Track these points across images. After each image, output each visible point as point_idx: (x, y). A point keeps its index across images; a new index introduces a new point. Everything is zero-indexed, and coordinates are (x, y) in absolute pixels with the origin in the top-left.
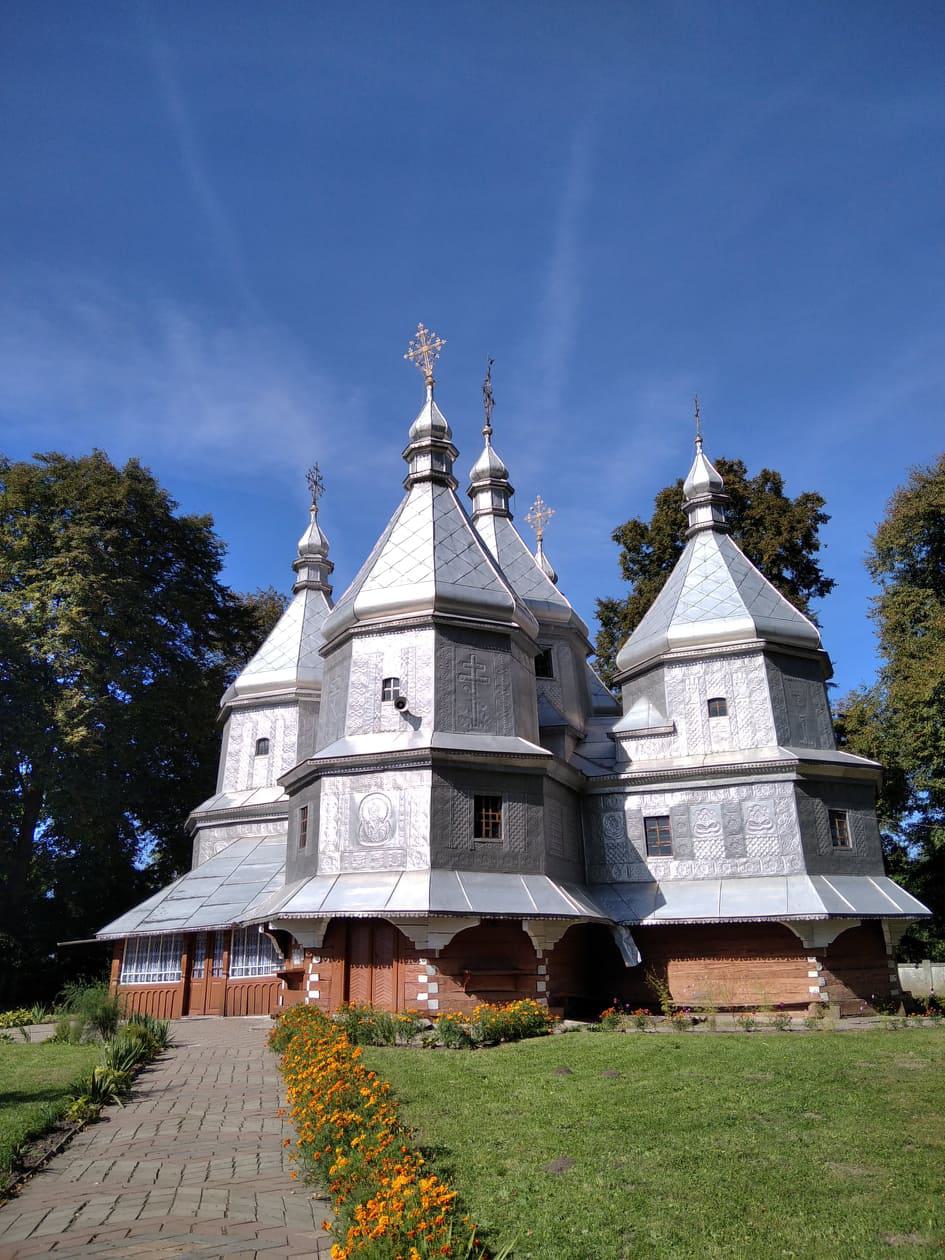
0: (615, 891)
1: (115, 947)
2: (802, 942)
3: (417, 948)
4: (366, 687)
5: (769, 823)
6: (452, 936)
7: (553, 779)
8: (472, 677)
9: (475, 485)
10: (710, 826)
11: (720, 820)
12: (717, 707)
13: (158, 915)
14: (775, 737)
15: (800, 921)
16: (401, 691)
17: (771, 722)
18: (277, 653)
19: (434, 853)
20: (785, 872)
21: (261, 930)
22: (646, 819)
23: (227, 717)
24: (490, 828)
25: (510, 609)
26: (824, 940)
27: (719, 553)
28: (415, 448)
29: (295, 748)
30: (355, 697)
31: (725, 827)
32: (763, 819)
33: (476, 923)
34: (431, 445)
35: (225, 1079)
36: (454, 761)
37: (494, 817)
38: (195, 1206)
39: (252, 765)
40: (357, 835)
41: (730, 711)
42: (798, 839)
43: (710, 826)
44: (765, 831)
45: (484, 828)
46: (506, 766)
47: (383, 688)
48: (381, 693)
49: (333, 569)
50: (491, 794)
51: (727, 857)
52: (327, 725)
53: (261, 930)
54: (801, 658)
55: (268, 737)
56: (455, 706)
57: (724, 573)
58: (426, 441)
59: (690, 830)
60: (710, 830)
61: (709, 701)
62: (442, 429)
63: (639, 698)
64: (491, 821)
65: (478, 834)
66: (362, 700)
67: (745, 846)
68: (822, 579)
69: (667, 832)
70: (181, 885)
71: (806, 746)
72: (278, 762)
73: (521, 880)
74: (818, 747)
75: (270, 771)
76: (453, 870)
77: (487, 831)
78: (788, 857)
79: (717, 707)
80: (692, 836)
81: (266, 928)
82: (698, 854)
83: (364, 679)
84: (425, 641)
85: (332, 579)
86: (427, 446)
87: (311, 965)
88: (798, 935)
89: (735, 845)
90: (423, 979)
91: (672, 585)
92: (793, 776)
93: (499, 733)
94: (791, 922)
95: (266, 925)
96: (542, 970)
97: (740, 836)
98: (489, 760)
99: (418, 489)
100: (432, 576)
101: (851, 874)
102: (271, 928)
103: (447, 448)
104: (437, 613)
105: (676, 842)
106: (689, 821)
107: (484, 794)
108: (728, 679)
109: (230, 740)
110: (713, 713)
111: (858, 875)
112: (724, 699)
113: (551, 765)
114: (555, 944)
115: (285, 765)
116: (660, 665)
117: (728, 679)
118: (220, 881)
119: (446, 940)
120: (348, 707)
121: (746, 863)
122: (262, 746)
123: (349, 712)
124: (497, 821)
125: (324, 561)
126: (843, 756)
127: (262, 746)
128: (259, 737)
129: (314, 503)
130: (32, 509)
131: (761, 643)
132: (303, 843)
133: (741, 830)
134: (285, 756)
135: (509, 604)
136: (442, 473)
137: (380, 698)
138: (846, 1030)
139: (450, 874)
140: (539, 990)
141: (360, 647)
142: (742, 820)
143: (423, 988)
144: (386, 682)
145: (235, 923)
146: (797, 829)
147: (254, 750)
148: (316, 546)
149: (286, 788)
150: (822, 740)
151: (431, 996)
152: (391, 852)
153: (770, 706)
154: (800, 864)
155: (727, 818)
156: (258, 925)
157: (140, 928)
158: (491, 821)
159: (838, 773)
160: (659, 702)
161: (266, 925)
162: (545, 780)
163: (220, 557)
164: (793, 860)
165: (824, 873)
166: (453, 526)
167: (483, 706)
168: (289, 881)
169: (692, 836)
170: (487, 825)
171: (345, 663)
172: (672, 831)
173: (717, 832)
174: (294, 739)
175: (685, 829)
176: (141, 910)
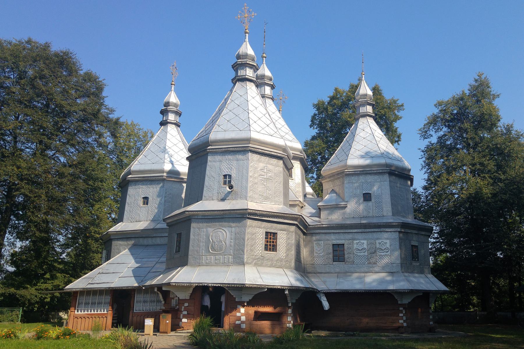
0: (318, 277)
1: (75, 294)
3: (237, 300)
6: (253, 295)
8: (265, 177)
13: (96, 280)
15: (182, 286)
22: (333, 245)
26: (406, 301)
28: (239, 64)
33: (422, 294)
37: (267, 242)
44: (385, 253)
45: (269, 247)
50: (273, 231)
60: (362, 251)
61: (363, 194)
65: (266, 249)
68: (79, 73)
77: (270, 248)
82: (356, 262)
87: (183, 307)
88: (396, 298)
90: (401, 315)
92: (399, 230)
94: (393, 292)
96: (290, 311)
105: (346, 256)
114: (296, 300)
116: (245, 151)
118: (148, 269)
119: (250, 297)
122: (146, 200)
124: (275, 244)
127: (146, 200)
132: (178, 251)
138: (431, 335)
140: (169, 316)
142: (376, 248)
143: (402, 318)
144: (225, 176)
157: (87, 287)
158: (272, 244)
163: (497, 107)
173: (364, 252)
176: (315, 285)
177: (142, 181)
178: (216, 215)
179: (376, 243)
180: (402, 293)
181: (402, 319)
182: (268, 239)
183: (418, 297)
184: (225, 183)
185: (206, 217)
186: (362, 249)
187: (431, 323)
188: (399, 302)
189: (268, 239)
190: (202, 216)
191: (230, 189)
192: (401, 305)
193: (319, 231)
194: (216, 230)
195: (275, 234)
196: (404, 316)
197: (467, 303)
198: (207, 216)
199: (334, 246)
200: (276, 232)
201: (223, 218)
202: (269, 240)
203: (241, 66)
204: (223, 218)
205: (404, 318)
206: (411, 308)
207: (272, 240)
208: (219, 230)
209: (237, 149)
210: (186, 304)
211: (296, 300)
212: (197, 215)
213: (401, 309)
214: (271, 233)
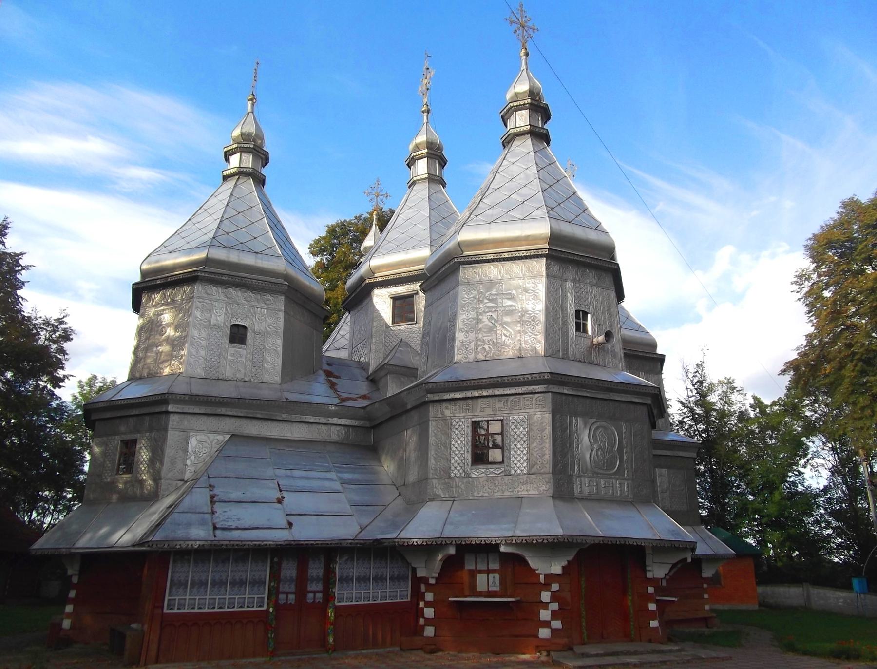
12: (238, 334)
22: (654, 455)
112: (245, 328)
151: (546, 624)
199: (501, 460)
210: (555, 587)
211: (563, 567)
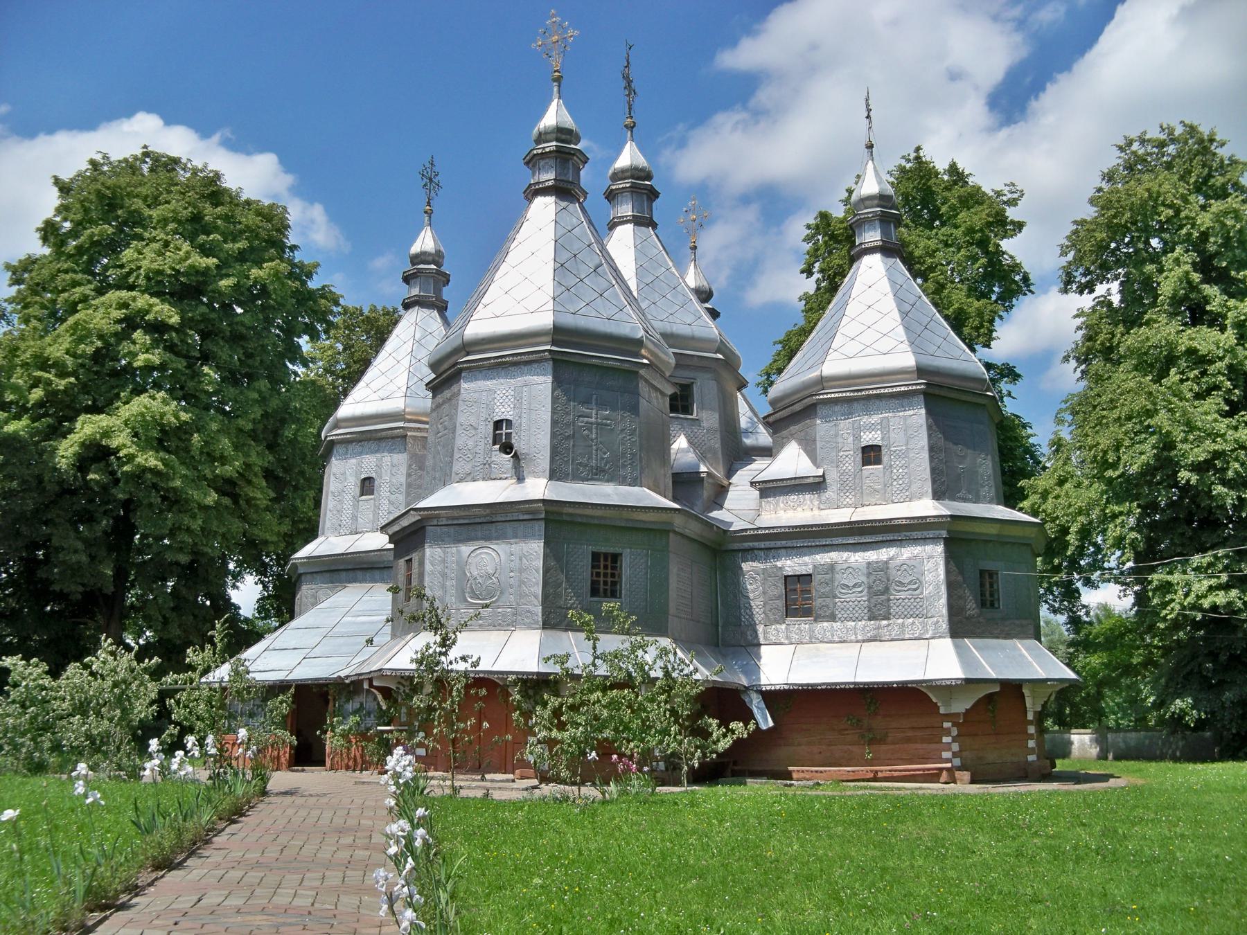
2: (938, 708)
4: (475, 429)
5: (860, 586)
7: (683, 536)
8: (593, 420)
9: (614, 187)
10: (854, 586)
11: (864, 579)
14: (930, 490)
16: (513, 435)
17: (927, 474)
18: (383, 380)
19: (545, 613)
20: (927, 636)
21: (366, 686)
22: (786, 577)
23: (327, 456)
24: (608, 587)
25: (639, 343)
26: (960, 706)
27: (886, 278)
28: (537, 154)
29: (403, 489)
30: (462, 440)
31: (870, 587)
32: (910, 579)
33: (997, 689)
34: (556, 151)
35: (325, 820)
36: (571, 515)
37: (613, 575)
38: (290, 899)
39: (355, 506)
40: (463, 592)
41: (885, 459)
42: (945, 596)
43: (854, 586)
44: (910, 592)
46: (627, 520)
47: (494, 431)
48: (491, 436)
49: (448, 281)
50: (611, 550)
51: (870, 619)
52: (434, 469)
53: (366, 686)
54: (965, 402)
55: (373, 475)
56: (573, 452)
57: (890, 304)
58: (551, 146)
59: (832, 591)
60: (854, 590)
62: (569, 132)
63: (789, 441)
64: (609, 580)
66: (471, 443)
67: (889, 608)
69: (809, 592)
70: (288, 635)
71: (965, 500)
72: (385, 505)
73: (1018, 643)
74: (977, 500)
75: (375, 514)
76: (566, 630)
77: (605, 590)
78: (932, 619)
79: (871, 454)
80: (835, 597)
81: (371, 685)
82: (840, 616)
83: (472, 420)
84: (541, 384)
85: (447, 293)
86: (550, 152)
88: (934, 700)
89: (878, 607)
90: (946, 739)
91: (832, 313)
93: (623, 482)
95: (370, 680)
97: (883, 597)
98: (608, 513)
99: (540, 201)
100: (550, 306)
101: (997, 638)
102: (375, 683)
103: (574, 155)
104: (554, 348)
105: (818, 603)
106: (832, 580)
107: (603, 550)
108: (884, 426)
109: (332, 478)
110: (866, 461)
111: (1005, 638)
113: (678, 521)
115: (392, 508)
117: (884, 426)
118: (324, 631)
120: (456, 450)
121: (889, 625)
122: (367, 486)
123: (456, 455)
124: (616, 579)
125: (439, 273)
126: (1002, 512)
128: (363, 476)
129: (429, 204)
130: (232, 547)
131: (920, 384)
133: (886, 590)
134: (393, 498)
135: (639, 336)
136: (569, 182)
137: (491, 442)
139: (563, 635)
141: (468, 388)
142: (888, 580)
143: (948, 747)
144: (498, 424)
145: (339, 677)
146: (943, 589)
147: (358, 490)
148: (430, 254)
149: (390, 537)
150: (983, 493)
152: (500, 610)
153: (927, 456)
154: (944, 626)
155: (873, 578)
156: (362, 680)
158: (609, 580)
159: (993, 530)
160: (810, 449)
161: (370, 680)
162: (671, 535)
164: (938, 622)
165: (967, 637)
166: (577, 246)
167: (605, 453)
168: (394, 636)
169: (835, 597)
170: (605, 583)
171: (453, 402)
172: (813, 591)
173: (861, 592)
174: (403, 479)
175: (827, 589)
177: (360, 441)
178: (476, 516)
179: (887, 568)
180: (948, 689)
181: (949, 749)
182: (599, 568)
183: (990, 698)
184: (494, 443)
185: (455, 522)
186: (856, 584)
187: (1032, 758)
188: (942, 711)
189: (599, 568)
190: (448, 518)
191: (508, 453)
192: (948, 717)
193: (751, 544)
194: (478, 552)
195: (615, 558)
196: (954, 741)
197: (140, 732)
198: (457, 518)
200: (618, 550)
201: (492, 522)
202: (602, 571)
203: (543, 159)
204: (492, 522)
205: (955, 747)
206: (969, 724)
207: (609, 571)
208: (485, 550)
209: (525, 358)
212: (437, 517)
213: (947, 725)
214: (606, 555)
